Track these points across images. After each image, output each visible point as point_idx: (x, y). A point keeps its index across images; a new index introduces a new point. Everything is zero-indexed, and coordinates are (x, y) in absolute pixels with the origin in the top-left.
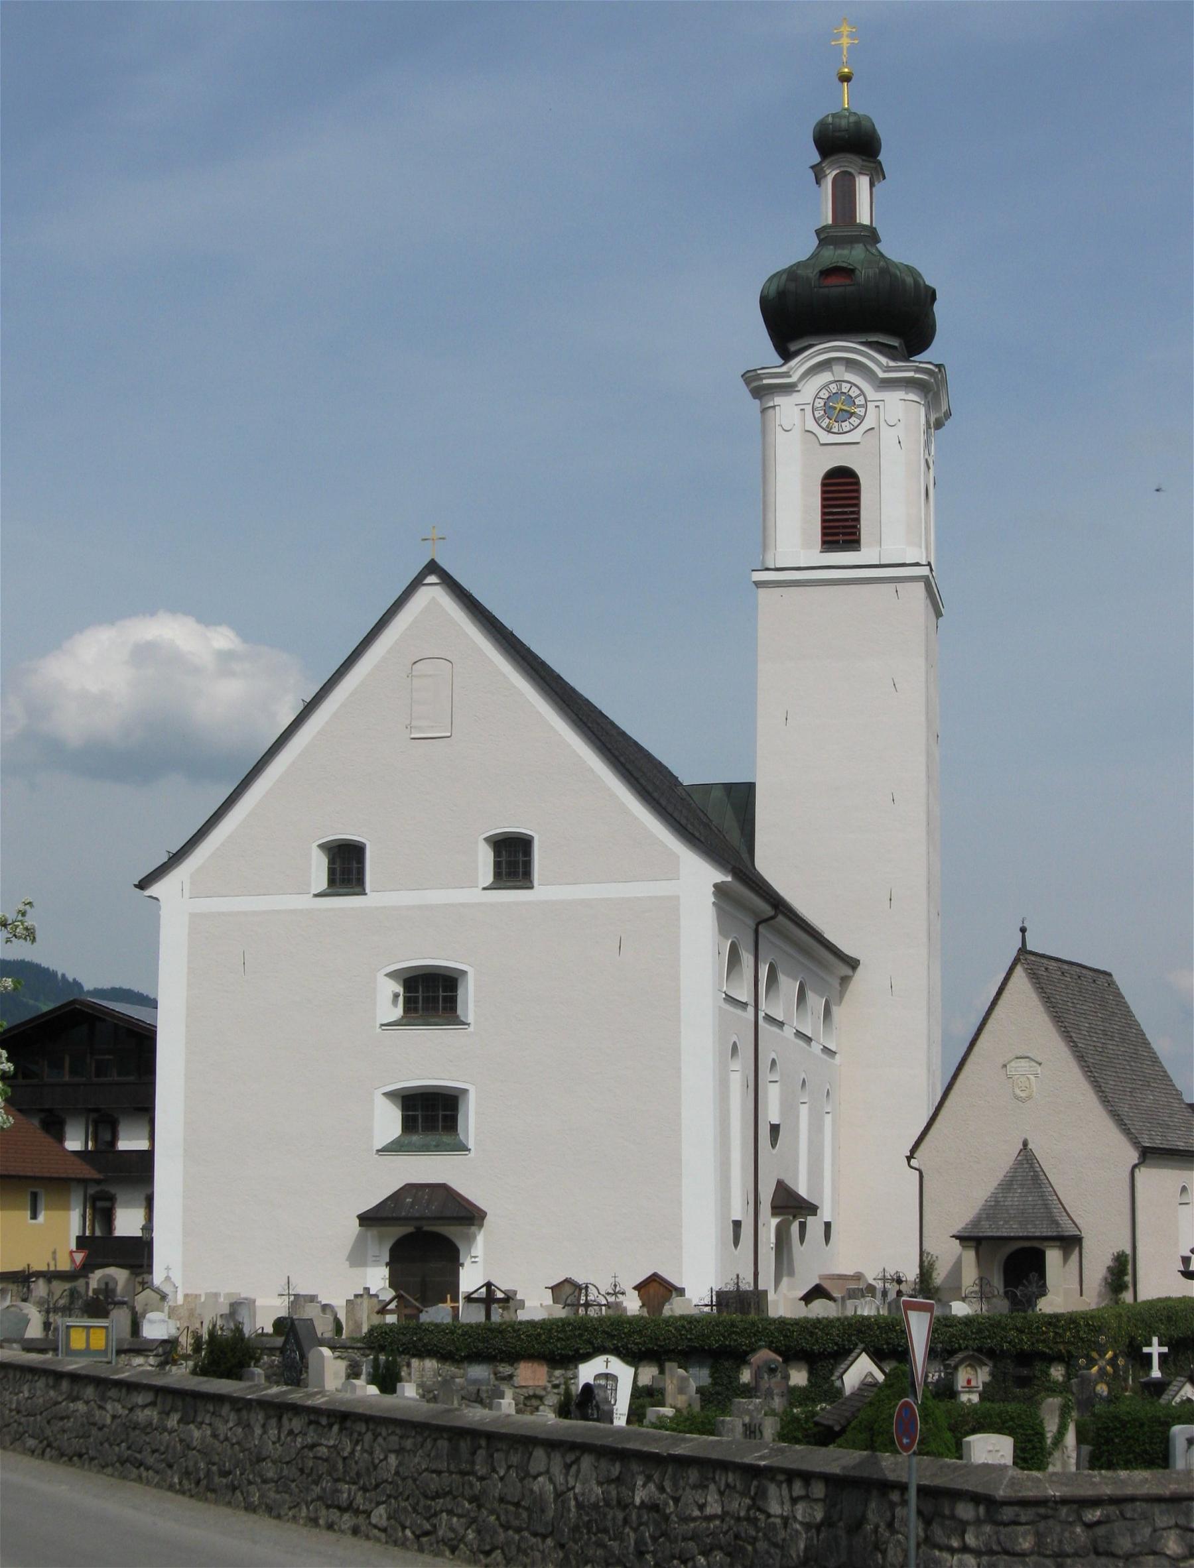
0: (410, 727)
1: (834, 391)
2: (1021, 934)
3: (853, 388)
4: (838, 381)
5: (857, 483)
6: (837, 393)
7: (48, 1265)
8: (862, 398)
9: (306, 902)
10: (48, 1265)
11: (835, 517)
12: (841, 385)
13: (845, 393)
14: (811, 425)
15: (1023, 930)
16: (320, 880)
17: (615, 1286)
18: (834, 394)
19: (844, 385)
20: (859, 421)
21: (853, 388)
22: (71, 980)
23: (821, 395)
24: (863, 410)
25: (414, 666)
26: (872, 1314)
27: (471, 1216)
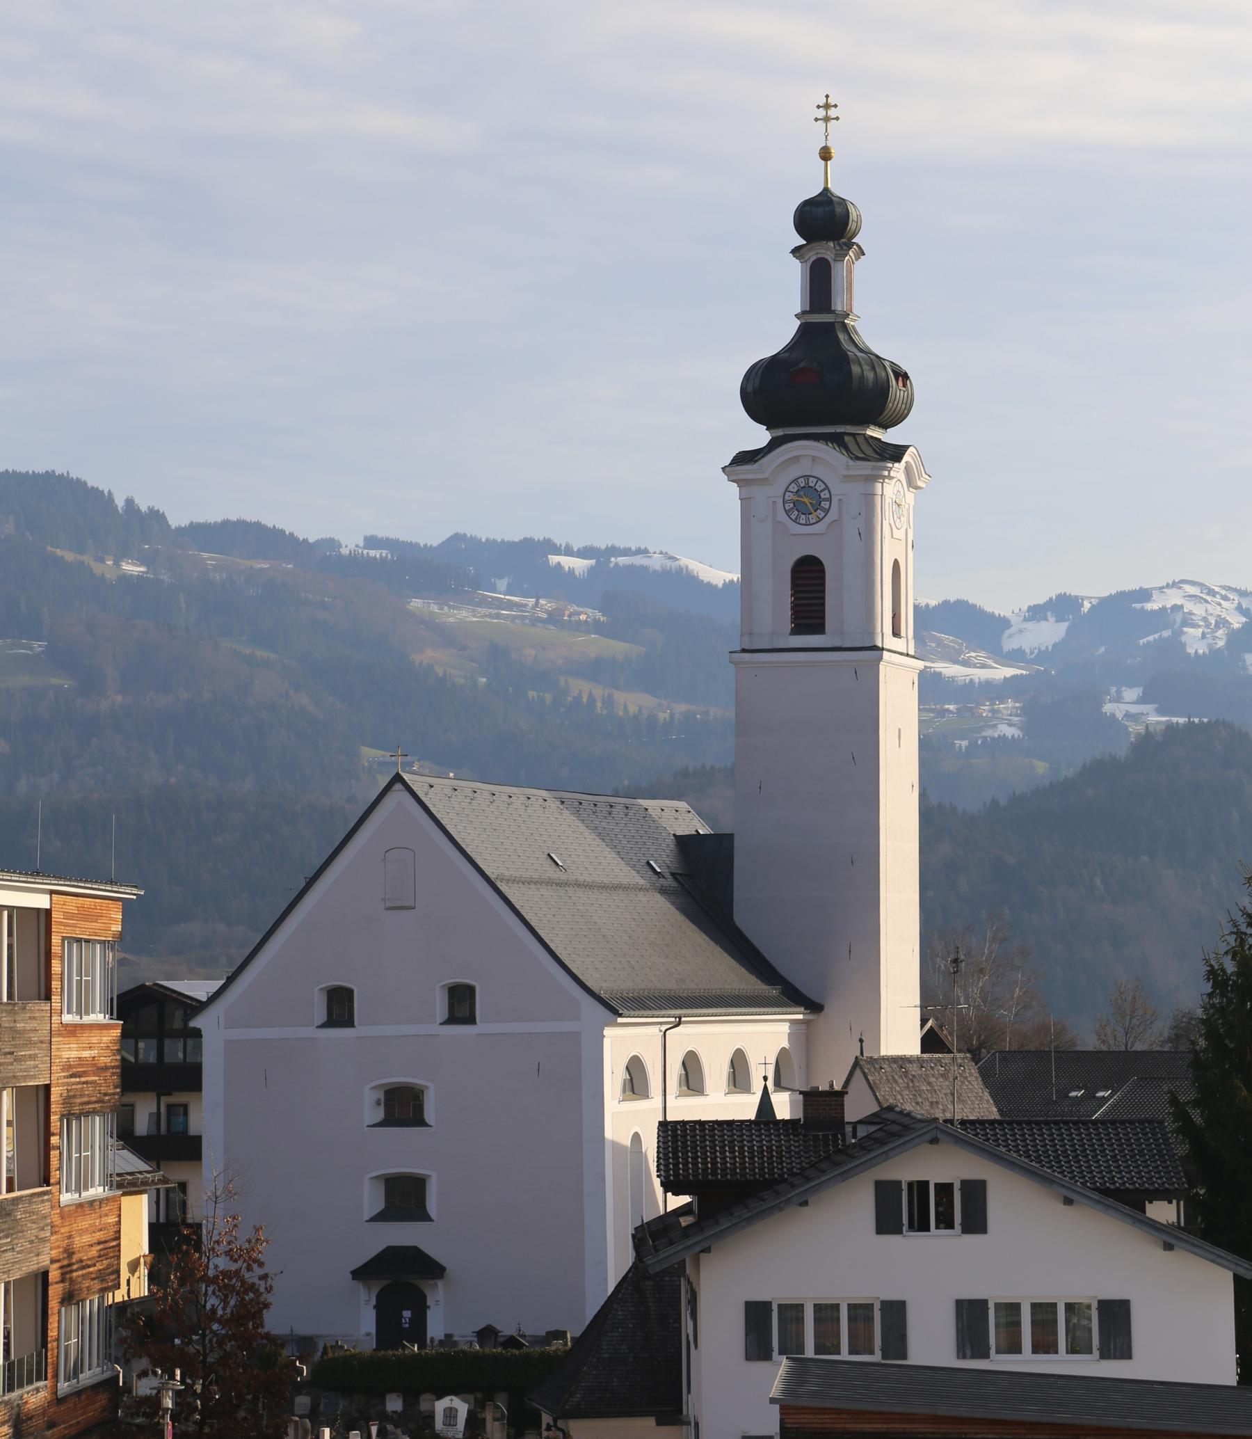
0: (384, 899)
1: (802, 485)
2: (859, 1044)
3: (819, 482)
4: (805, 476)
5: (823, 571)
6: (805, 487)
7: (123, 1296)
8: (826, 492)
9: (310, 1032)
10: (123, 1296)
11: (806, 602)
12: (808, 479)
13: (811, 487)
14: (782, 516)
15: (861, 1041)
16: (321, 1015)
17: (520, 1330)
18: (802, 488)
19: (811, 479)
20: (824, 514)
21: (819, 482)
22: (144, 508)
23: (791, 488)
24: (828, 503)
25: (387, 854)
26: (296, 1408)
27: (434, 1270)
